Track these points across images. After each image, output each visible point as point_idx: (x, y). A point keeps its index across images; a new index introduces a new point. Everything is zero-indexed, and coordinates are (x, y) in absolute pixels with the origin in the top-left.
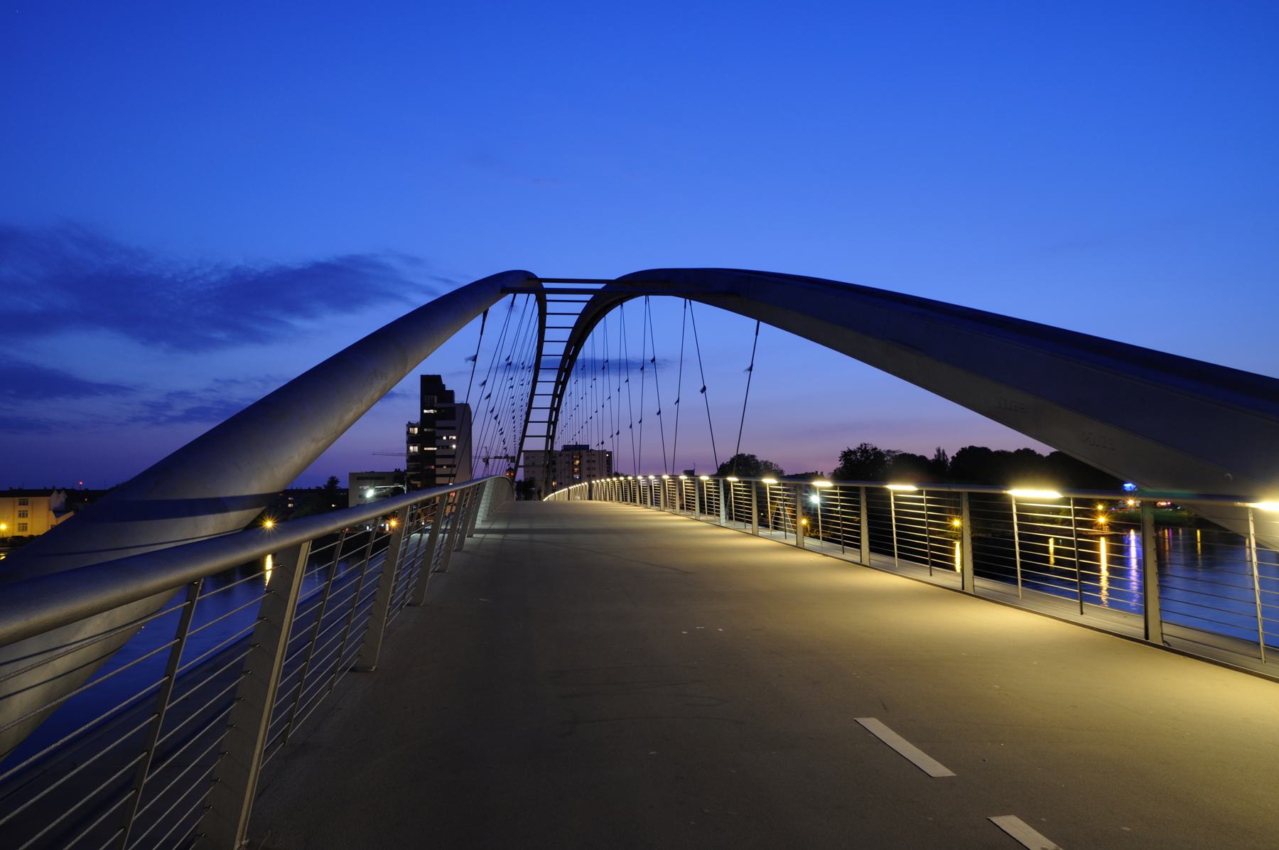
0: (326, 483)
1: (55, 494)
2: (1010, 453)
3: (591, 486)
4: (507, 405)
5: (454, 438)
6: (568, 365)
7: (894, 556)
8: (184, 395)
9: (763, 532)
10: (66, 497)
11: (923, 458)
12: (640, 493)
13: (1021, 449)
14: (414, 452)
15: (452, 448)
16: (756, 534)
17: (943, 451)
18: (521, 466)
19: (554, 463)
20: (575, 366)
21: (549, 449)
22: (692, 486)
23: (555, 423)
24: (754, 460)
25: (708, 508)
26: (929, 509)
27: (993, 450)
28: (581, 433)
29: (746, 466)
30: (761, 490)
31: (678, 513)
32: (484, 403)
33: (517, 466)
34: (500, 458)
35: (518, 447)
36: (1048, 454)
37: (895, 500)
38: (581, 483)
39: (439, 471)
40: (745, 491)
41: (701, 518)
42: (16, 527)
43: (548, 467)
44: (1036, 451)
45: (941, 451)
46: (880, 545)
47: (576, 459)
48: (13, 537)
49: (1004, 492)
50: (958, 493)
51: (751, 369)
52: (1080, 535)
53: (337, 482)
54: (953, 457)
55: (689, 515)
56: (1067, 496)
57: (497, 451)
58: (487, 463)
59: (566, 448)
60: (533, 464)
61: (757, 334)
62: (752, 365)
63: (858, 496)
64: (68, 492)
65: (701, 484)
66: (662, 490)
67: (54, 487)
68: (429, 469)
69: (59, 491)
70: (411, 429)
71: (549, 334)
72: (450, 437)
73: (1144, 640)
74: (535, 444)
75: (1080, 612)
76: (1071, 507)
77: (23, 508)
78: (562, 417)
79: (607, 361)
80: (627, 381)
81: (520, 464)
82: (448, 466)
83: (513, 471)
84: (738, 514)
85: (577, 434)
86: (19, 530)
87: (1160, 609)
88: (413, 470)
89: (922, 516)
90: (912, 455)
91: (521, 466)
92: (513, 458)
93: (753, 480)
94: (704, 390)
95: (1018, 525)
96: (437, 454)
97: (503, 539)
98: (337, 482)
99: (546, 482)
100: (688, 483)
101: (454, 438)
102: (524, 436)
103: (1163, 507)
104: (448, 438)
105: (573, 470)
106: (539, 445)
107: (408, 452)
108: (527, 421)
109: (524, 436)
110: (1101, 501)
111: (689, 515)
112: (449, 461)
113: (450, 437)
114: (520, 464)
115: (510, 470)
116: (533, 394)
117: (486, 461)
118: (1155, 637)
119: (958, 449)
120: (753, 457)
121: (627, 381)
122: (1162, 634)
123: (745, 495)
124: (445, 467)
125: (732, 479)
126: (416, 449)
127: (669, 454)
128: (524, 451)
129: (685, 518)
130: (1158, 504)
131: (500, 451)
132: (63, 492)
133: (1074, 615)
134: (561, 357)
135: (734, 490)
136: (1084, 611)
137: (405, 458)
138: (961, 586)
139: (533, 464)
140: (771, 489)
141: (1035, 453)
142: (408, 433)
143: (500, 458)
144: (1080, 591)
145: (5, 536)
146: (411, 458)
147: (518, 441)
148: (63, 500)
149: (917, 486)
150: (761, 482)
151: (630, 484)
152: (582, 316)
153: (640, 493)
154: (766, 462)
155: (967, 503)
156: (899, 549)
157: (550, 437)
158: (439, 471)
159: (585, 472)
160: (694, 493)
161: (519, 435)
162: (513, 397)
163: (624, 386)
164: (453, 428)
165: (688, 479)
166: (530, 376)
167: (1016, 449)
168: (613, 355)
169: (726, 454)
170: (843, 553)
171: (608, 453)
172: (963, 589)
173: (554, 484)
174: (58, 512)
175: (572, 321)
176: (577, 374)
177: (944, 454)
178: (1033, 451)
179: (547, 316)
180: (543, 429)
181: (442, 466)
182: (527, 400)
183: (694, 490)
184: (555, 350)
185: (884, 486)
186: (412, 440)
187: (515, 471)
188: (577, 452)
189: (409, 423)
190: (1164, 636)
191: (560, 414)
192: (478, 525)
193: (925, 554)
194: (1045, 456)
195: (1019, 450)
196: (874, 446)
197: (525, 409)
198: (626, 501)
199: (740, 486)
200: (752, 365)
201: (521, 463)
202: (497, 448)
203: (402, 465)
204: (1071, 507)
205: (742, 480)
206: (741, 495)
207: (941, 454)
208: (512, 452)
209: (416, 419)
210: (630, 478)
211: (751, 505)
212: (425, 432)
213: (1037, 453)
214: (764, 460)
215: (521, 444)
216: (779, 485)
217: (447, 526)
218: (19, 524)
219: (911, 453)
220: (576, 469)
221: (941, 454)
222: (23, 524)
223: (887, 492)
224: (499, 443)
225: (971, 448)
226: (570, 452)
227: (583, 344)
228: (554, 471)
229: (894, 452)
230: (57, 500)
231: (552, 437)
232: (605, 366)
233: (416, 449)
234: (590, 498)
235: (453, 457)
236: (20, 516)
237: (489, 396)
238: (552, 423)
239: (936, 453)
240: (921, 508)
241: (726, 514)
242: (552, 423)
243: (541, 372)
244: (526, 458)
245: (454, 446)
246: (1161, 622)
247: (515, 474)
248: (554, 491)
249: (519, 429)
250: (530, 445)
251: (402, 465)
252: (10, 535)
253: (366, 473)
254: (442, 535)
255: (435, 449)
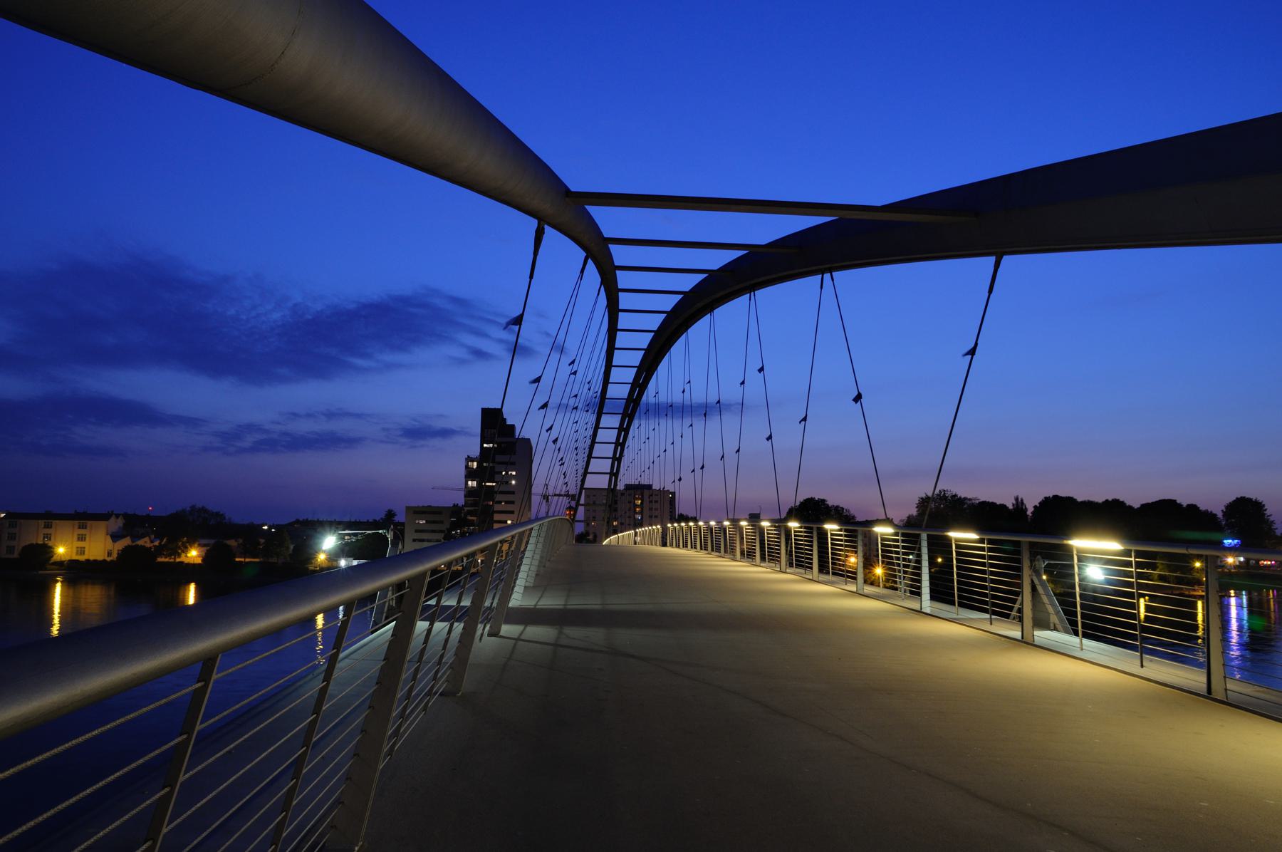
0: (383, 516)
1: (113, 519)
2: (1097, 503)
3: (665, 530)
4: (562, 508)
5: (514, 473)
6: (632, 408)
7: (955, 605)
8: (251, 428)
9: (823, 577)
10: (124, 521)
11: (1003, 507)
12: (691, 537)
13: (1110, 499)
14: (472, 487)
15: (511, 484)
16: (1029, 640)
17: (1022, 500)
18: (582, 505)
19: (616, 502)
20: (638, 410)
21: (612, 487)
22: (775, 534)
23: (619, 460)
24: (825, 504)
25: (769, 555)
26: (991, 558)
27: (1079, 500)
28: (642, 476)
29: (813, 511)
30: (822, 535)
31: (723, 555)
32: (545, 435)
33: (578, 504)
34: (559, 495)
35: (579, 483)
36: (1139, 506)
37: (881, 540)
38: (651, 525)
39: (497, 507)
40: (805, 536)
41: (788, 571)
42: (75, 551)
43: (610, 506)
44: (1126, 502)
45: (1020, 500)
46: (941, 593)
47: (638, 499)
48: (70, 561)
49: (1066, 542)
50: (1019, 542)
51: (972, 352)
52: (904, 560)
53: (394, 515)
54: (1035, 507)
55: (801, 573)
56: (898, 531)
57: (555, 488)
58: (547, 501)
59: (628, 487)
60: (594, 503)
61: (990, 291)
62: (976, 344)
63: (1019, 553)
64: (126, 516)
65: (761, 530)
66: (722, 534)
67: (112, 512)
68: (488, 505)
69: (117, 516)
70: (470, 463)
71: (621, 340)
72: (510, 473)
73: (1206, 694)
74: (598, 481)
75: (1140, 665)
76: (1133, 559)
77: (82, 531)
78: (628, 452)
79: (671, 406)
80: (691, 425)
81: (581, 503)
82: (506, 502)
83: (573, 509)
84: (799, 561)
85: (647, 470)
86: (77, 554)
87: (1223, 665)
88: (472, 505)
89: (983, 564)
90: (992, 503)
91: (582, 505)
92: (573, 497)
93: (815, 526)
94: (858, 398)
95: (956, 559)
96: (496, 489)
97: (556, 645)
98: (394, 515)
99: (608, 522)
100: (749, 529)
101: (514, 473)
102: (586, 472)
103: (1267, 566)
104: (507, 473)
105: (635, 510)
106: (600, 482)
107: (466, 487)
108: (590, 457)
109: (586, 472)
110: (1199, 557)
111: (801, 573)
112: (510, 497)
113: (510, 473)
114: (581, 503)
115: (570, 508)
116: (593, 442)
117: (546, 497)
118: (1218, 692)
119: (1041, 498)
120: (823, 501)
121: (691, 425)
122: (1226, 690)
123: (806, 541)
124: (503, 503)
125: (793, 525)
126: (475, 483)
127: (731, 496)
128: (585, 489)
129: (764, 569)
130: (1260, 563)
131: (559, 487)
132: (121, 517)
133: (1134, 667)
134: (625, 401)
135: (832, 539)
136: (1144, 664)
137: (462, 494)
138: (1205, 686)
139: (594, 503)
140: (832, 535)
141: (1125, 504)
142: (467, 467)
143: (559, 495)
144: (1141, 644)
145: (63, 559)
146: (470, 493)
147: (580, 478)
148: (121, 525)
149: (839, 526)
150: (824, 528)
151: (700, 530)
152: (658, 334)
153: (691, 537)
154: (837, 507)
155: (1028, 553)
156: (959, 597)
157: (614, 474)
158: (497, 507)
159: (646, 512)
160: (755, 539)
161: (581, 471)
162: (576, 422)
163: (687, 432)
164: (513, 464)
165: (749, 526)
166: (591, 418)
167: (1104, 500)
168: (677, 398)
169: (790, 498)
170: (991, 624)
171: (671, 493)
172: (1022, 638)
173: (614, 523)
174: (115, 537)
175: (655, 322)
176: (640, 419)
177: (1022, 503)
178: (1123, 502)
179: (615, 351)
180: (606, 466)
181: (500, 502)
182: (591, 432)
183: (755, 536)
184: (619, 391)
185: (1066, 542)
186: (470, 474)
187: (576, 510)
188: (639, 492)
189: (468, 456)
190: (1228, 692)
191: (626, 450)
192: (517, 600)
193: (986, 603)
194: (1185, 505)
195: (1107, 500)
196: (954, 494)
197: (589, 442)
198: (696, 548)
199: (841, 535)
200: (976, 344)
201: (582, 501)
202: (556, 485)
203: (460, 500)
204: (1133, 559)
205: (986, 537)
206: (801, 540)
207: (1020, 505)
208: (573, 490)
209: (476, 452)
210: (713, 523)
211: (812, 551)
212: (485, 466)
213: (1185, 505)
214: (835, 505)
215: (583, 481)
216: (801, 527)
217: (429, 631)
218: (77, 548)
219: (991, 501)
220: (638, 509)
221: (1020, 505)
222: (81, 548)
223: (949, 540)
224: (558, 478)
225: (1056, 497)
226: (632, 492)
227: (657, 368)
228: (616, 510)
229: (970, 499)
230: (116, 524)
231: (616, 475)
232: (669, 410)
233: (475, 483)
234: (664, 544)
235: (513, 493)
236: (78, 539)
237: (550, 428)
238: (617, 459)
239: (1014, 502)
240: (983, 557)
241: (786, 561)
242: (617, 459)
243: (604, 417)
244: (587, 496)
245: (513, 482)
246: (1225, 677)
247: (575, 513)
248: (615, 532)
249: (582, 464)
250: (592, 482)
251: (460, 500)
252: (68, 558)
253: (423, 506)
254: (462, 604)
255: (494, 484)
